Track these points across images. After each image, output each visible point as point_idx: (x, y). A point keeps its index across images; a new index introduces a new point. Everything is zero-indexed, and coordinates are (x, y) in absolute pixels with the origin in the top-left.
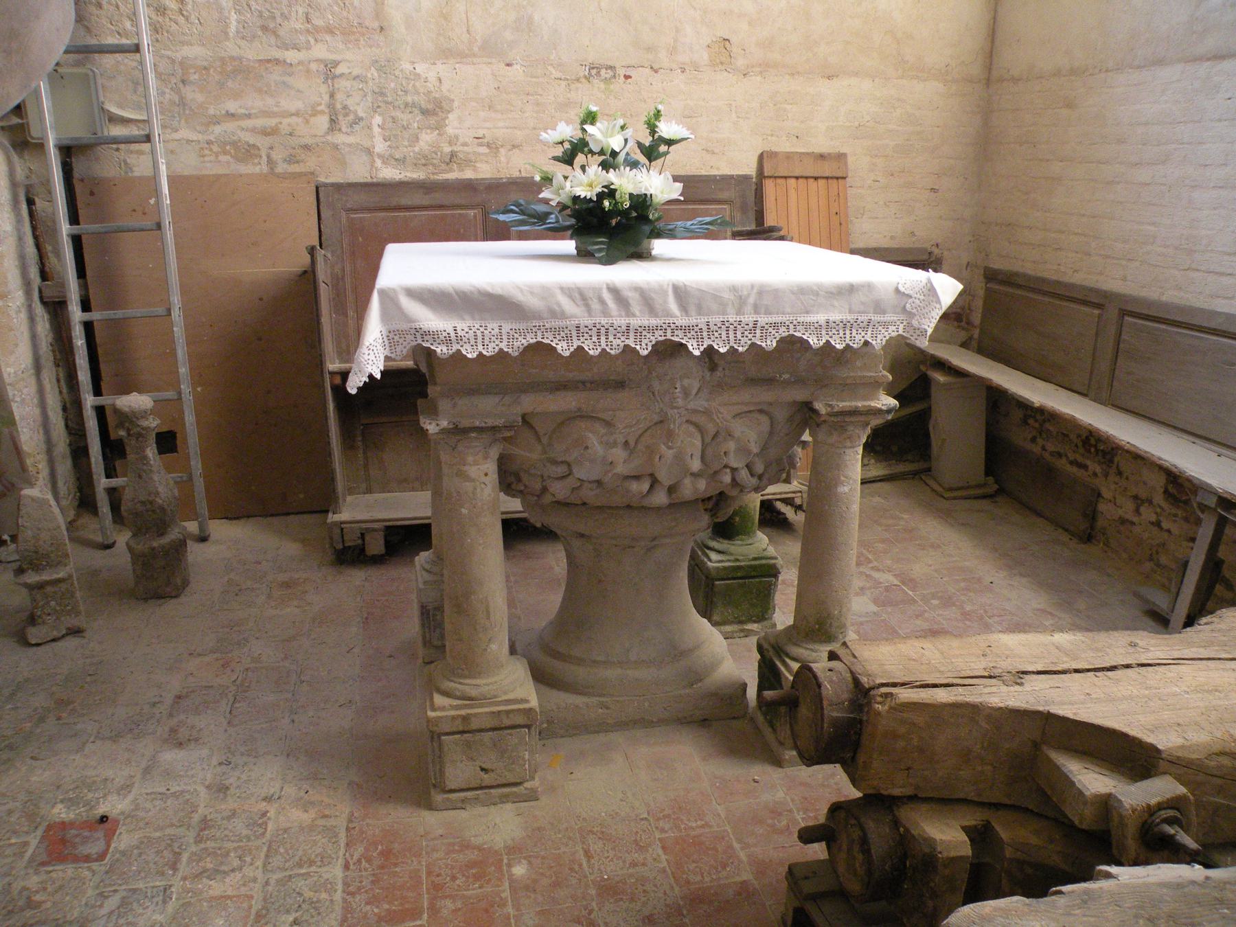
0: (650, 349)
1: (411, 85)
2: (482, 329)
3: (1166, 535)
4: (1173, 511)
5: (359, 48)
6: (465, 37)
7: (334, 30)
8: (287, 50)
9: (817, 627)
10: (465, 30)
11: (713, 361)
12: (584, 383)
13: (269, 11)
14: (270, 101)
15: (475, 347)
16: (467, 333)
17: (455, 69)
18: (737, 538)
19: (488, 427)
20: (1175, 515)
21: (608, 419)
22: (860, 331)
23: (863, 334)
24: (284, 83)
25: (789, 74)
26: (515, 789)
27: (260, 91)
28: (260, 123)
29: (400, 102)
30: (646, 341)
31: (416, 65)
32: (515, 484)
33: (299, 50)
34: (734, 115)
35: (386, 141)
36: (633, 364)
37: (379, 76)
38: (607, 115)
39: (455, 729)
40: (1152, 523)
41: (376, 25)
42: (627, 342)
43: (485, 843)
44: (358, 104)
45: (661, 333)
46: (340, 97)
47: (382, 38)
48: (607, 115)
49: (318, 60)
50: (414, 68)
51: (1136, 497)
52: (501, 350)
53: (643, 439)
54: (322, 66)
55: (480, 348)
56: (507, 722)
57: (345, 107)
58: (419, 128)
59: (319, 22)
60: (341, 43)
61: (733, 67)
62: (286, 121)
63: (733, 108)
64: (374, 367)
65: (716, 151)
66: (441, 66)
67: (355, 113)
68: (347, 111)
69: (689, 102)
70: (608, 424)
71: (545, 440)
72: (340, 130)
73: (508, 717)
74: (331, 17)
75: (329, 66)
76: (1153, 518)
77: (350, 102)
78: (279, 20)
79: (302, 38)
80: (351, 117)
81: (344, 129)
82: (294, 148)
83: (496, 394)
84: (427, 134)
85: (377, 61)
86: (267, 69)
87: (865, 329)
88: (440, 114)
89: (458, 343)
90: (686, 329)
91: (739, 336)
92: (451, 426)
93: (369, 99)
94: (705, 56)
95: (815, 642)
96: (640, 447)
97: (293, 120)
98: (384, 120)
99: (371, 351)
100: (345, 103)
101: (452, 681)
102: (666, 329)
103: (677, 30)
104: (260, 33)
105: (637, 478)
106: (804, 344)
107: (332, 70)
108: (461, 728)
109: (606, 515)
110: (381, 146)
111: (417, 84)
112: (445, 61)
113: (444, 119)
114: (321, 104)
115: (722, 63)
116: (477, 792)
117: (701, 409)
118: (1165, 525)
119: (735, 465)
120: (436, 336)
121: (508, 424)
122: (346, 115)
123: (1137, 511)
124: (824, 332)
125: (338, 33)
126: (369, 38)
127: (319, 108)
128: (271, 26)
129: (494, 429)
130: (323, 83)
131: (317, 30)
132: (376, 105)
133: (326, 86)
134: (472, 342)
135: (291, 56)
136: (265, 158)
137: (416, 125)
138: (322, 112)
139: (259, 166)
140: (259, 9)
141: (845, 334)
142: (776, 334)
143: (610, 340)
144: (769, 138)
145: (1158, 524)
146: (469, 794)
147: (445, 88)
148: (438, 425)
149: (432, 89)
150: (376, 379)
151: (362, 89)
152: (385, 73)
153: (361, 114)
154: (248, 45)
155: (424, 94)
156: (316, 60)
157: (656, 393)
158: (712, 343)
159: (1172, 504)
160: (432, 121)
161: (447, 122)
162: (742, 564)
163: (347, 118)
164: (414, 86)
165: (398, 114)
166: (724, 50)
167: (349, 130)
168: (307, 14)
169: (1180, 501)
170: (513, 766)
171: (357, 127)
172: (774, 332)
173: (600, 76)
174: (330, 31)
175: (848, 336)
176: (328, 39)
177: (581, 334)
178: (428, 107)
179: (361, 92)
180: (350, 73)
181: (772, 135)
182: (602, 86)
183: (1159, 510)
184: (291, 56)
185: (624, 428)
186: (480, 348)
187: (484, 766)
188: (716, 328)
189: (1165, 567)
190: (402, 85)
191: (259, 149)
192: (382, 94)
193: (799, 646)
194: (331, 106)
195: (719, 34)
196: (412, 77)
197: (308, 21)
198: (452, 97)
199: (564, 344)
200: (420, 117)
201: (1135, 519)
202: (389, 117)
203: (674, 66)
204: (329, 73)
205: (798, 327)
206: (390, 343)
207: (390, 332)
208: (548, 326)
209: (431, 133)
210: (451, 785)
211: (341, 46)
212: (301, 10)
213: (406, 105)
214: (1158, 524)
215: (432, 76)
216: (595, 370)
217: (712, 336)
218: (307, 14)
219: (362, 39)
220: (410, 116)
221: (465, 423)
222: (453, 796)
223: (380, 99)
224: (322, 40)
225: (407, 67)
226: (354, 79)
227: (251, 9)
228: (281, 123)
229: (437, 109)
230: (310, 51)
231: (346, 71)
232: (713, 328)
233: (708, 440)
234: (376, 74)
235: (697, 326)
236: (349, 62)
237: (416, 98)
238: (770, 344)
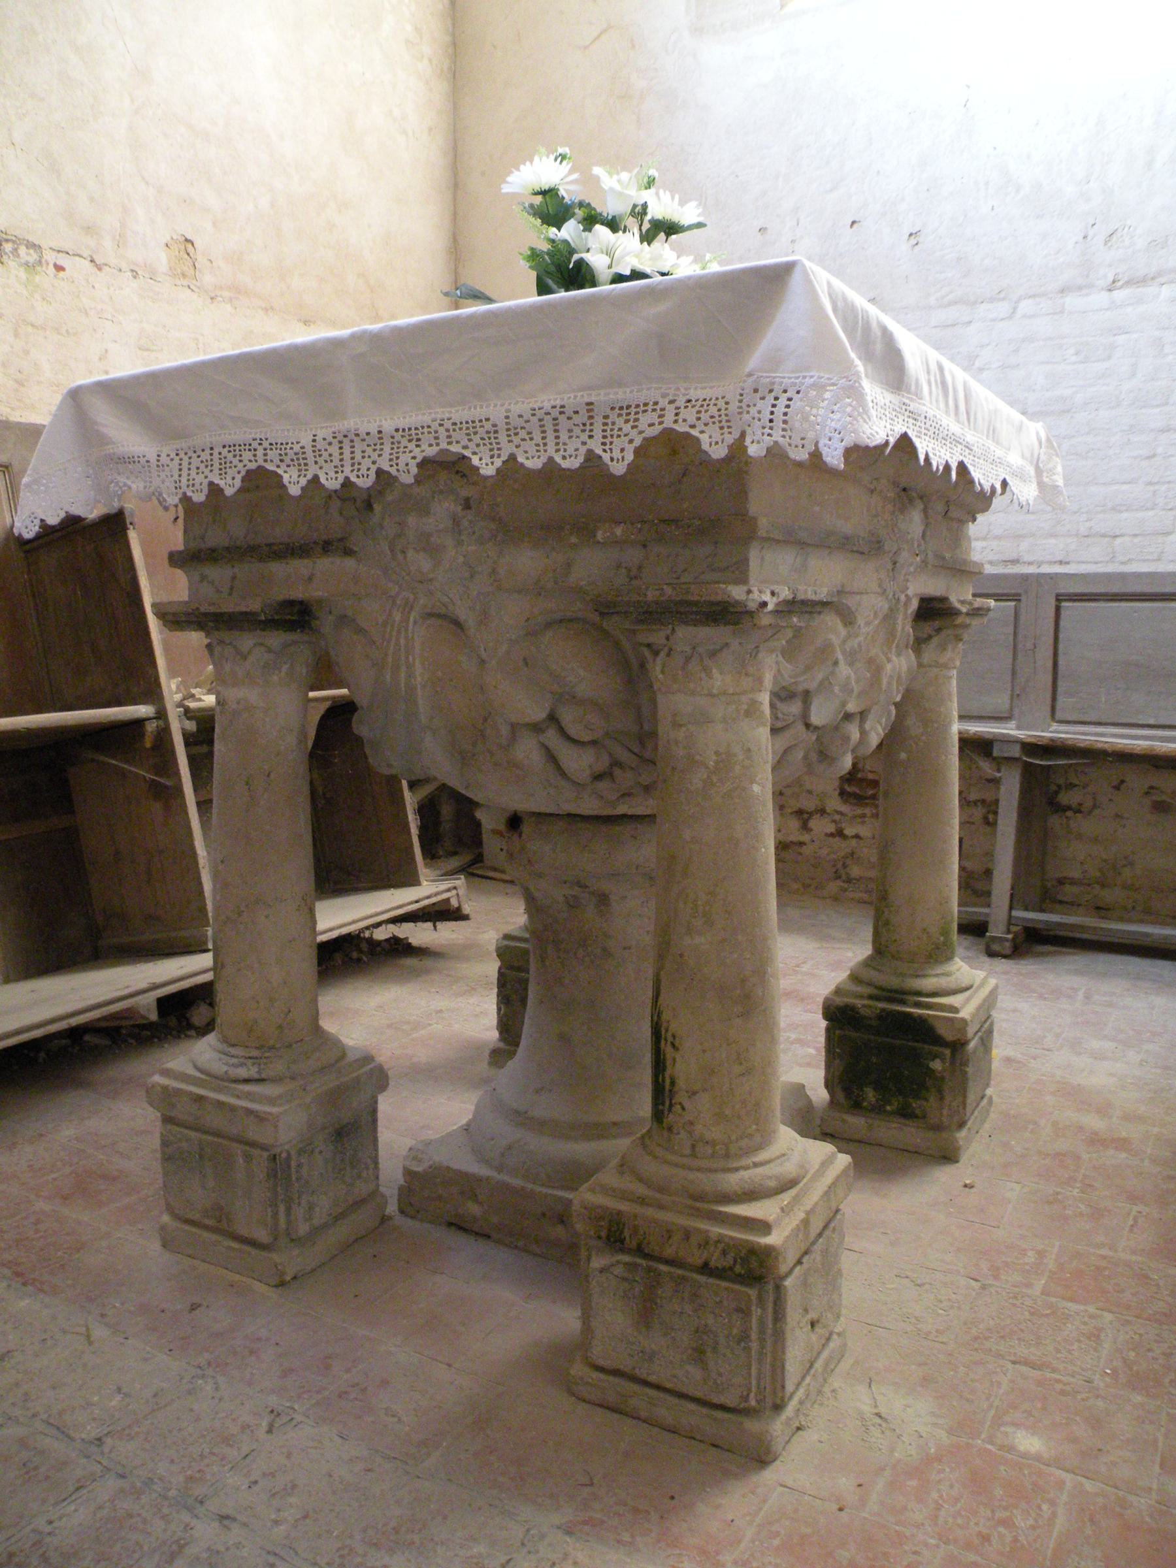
0: (630, 457)
3: (854, 842)
4: (859, 811)
9: (942, 938)
20: (863, 816)
22: (369, 450)
38: (32, 325)
40: (832, 835)
48: (32, 325)
51: (799, 813)
61: (198, 284)
76: (831, 828)
95: (941, 963)
101: (737, 1169)
118: (849, 831)
123: (805, 827)
124: (503, 438)
134: (336, 462)
143: (561, 441)
145: (840, 833)
159: (855, 805)
166: (186, 256)
169: (866, 798)
173: (18, 256)
182: (23, 274)
183: (837, 817)
189: (859, 879)
193: (925, 976)
201: (805, 838)
203: (124, 266)
214: (840, 833)
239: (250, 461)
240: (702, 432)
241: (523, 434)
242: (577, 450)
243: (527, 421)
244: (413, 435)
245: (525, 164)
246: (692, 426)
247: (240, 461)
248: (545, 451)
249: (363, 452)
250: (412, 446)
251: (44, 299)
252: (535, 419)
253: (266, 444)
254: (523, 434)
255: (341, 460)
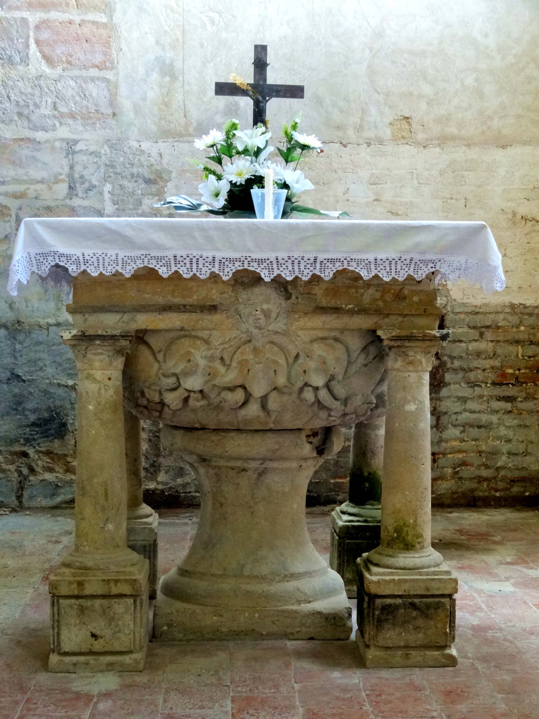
0: (231, 275)
1: (136, 159)
2: (103, 256)
5: (95, 130)
6: (183, 121)
7: (75, 116)
8: (37, 131)
9: (396, 535)
10: (182, 115)
11: (288, 292)
12: (184, 306)
13: (24, 101)
14: (21, 172)
15: (97, 268)
16: (92, 257)
17: (174, 146)
18: (367, 503)
19: (108, 336)
21: (206, 337)
22: (404, 267)
23: (406, 269)
24: (33, 157)
25: (465, 146)
26: (120, 658)
27: (13, 163)
28: (11, 188)
29: (127, 173)
30: (228, 269)
31: (141, 143)
32: (140, 399)
33: (46, 131)
34: (415, 182)
35: (114, 205)
36: (224, 293)
37: (111, 152)
39: (71, 593)
41: (110, 111)
42: (213, 270)
43: (82, 691)
44: (93, 175)
45: (240, 264)
46: (78, 168)
47: (114, 122)
49: (62, 140)
50: (140, 146)
52: (117, 271)
53: (235, 356)
54: (64, 144)
55: (101, 269)
56: (115, 591)
57: (82, 177)
58: (142, 194)
59: (63, 109)
60: (80, 126)
62: (33, 187)
63: (414, 176)
64: (22, 276)
65: (400, 212)
66: (162, 144)
67: (90, 181)
68: (84, 180)
69: (374, 171)
70: (207, 342)
71: (160, 357)
72: (77, 195)
73: (116, 585)
74: (73, 106)
75: (70, 144)
77: (86, 173)
78: (32, 108)
79: (50, 122)
80: (86, 185)
81: (80, 195)
82: (39, 209)
83: (116, 312)
84: (149, 199)
85: (109, 140)
86: (20, 146)
87: (408, 265)
88: (161, 183)
89: (85, 265)
90: (260, 261)
91: (302, 268)
92: (80, 334)
93: (102, 170)
94: (388, 132)
96: (234, 364)
97: (39, 187)
98: (113, 187)
99: (20, 264)
100: (82, 173)
102: (243, 261)
103: (363, 111)
104: (16, 118)
105: (231, 389)
106: (358, 278)
107: (73, 147)
108: (76, 592)
109: (220, 437)
110: (110, 209)
111: (142, 159)
112: (165, 140)
113: (163, 187)
114: (61, 174)
115: (403, 138)
116: (88, 658)
117: (280, 331)
119: (315, 384)
120: (69, 258)
121: (122, 334)
122: (83, 183)
124: (373, 267)
125: (79, 118)
126: (104, 122)
127: (61, 177)
128: (25, 113)
129: (113, 337)
130: (65, 157)
131: (62, 115)
132: (107, 175)
133: (67, 159)
134: (96, 265)
135: (40, 135)
136: (14, 216)
137: (140, 192)
138: (63, 181)
139: (9, 223)
140: (17, 99)
141: (390, 269)
142: (333, 268)
144: (449, 201)
146: (82, 659)
147: (165, 161)
148: (70, 333)
149: (155, 163)
150: (24, 284)
151: (96, 163)
152: (116, 150)
153: (95, 182)
154: (7, 127)
155: (147, 166)
156: (60, 139)
157: (242, 316)
158: (280, 273)
160: (154, 189)
161: (166, 189)
162: (370, 524)
163: (83, 186)
164: (139, 160)
165: (125, 183)
167: (84, 195)
168: (55, 103)
170: (119, 635)
171: (91, 193)
172: (331, 266)
174: (72, 116)
175: (393, 271)
176: (70, 123)
177: (178, 262)
178: (151, 177)
179: (95, 165)
180: (88, 149)
181: (451, 198)
184: (40, 135)
185: (219, 345)
186: (101, 269)
187: (95, 631)
188: (283, 262)
190: (129, 159)
191: (9, 209)
192: (113, 166)
194: (70, 176)
195: (400, 113)
196: (138, 153)
197: (55, 108)
198: (171, 169)
199: (165, 269)
200: (143, 186)
202: (118, 185)
203: (361, 141)
204: (70, 149)
205: (351, 263)
206: (37, 263)
207: (37, 254)
208: (152, 255)
209: (153, 199)
210: (66, 647)
211: (81, 128)
212: (49, 101)
213: (132, 175)
215: (154, 154)
216: (195, 297)
217: (280, 268)
218: (55, 103)
219: (98, 123)
220: (135, 184)
221: (90, 332)
222: (67, 659)
223: (111, 170)
224: (66, 124)
225: (135, 144)
226: (90, 154)
227: (10, 100)
228: (28, 189)
229: (158, 179)
230: (55, 132)
231: (84, 148)
232: (281, 261)
233: (291, 361)
234: (108, 151)
235: (268, 259)
236: (87, 140)
237: (140, 170)
238: (327, 275)
239: (52, 261)
240: (159, 269)
241: (182, 264)
242: (308, 273)
243: (185, 259)
244: (134, 260)
245: (213, 130)
246: (155, 266)
247: (47, 261)
248: (294, 273)
249: (401, 267)
250: (230, 265)
251: (310, 169)
252: (290, 261)
253: (149, 257)
254: (182, 264)
255: (98, 265)
